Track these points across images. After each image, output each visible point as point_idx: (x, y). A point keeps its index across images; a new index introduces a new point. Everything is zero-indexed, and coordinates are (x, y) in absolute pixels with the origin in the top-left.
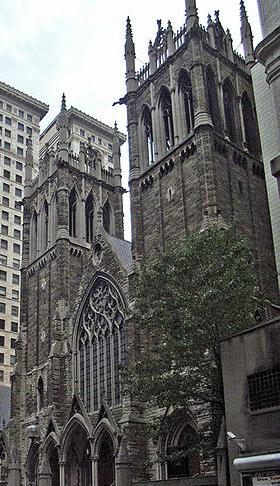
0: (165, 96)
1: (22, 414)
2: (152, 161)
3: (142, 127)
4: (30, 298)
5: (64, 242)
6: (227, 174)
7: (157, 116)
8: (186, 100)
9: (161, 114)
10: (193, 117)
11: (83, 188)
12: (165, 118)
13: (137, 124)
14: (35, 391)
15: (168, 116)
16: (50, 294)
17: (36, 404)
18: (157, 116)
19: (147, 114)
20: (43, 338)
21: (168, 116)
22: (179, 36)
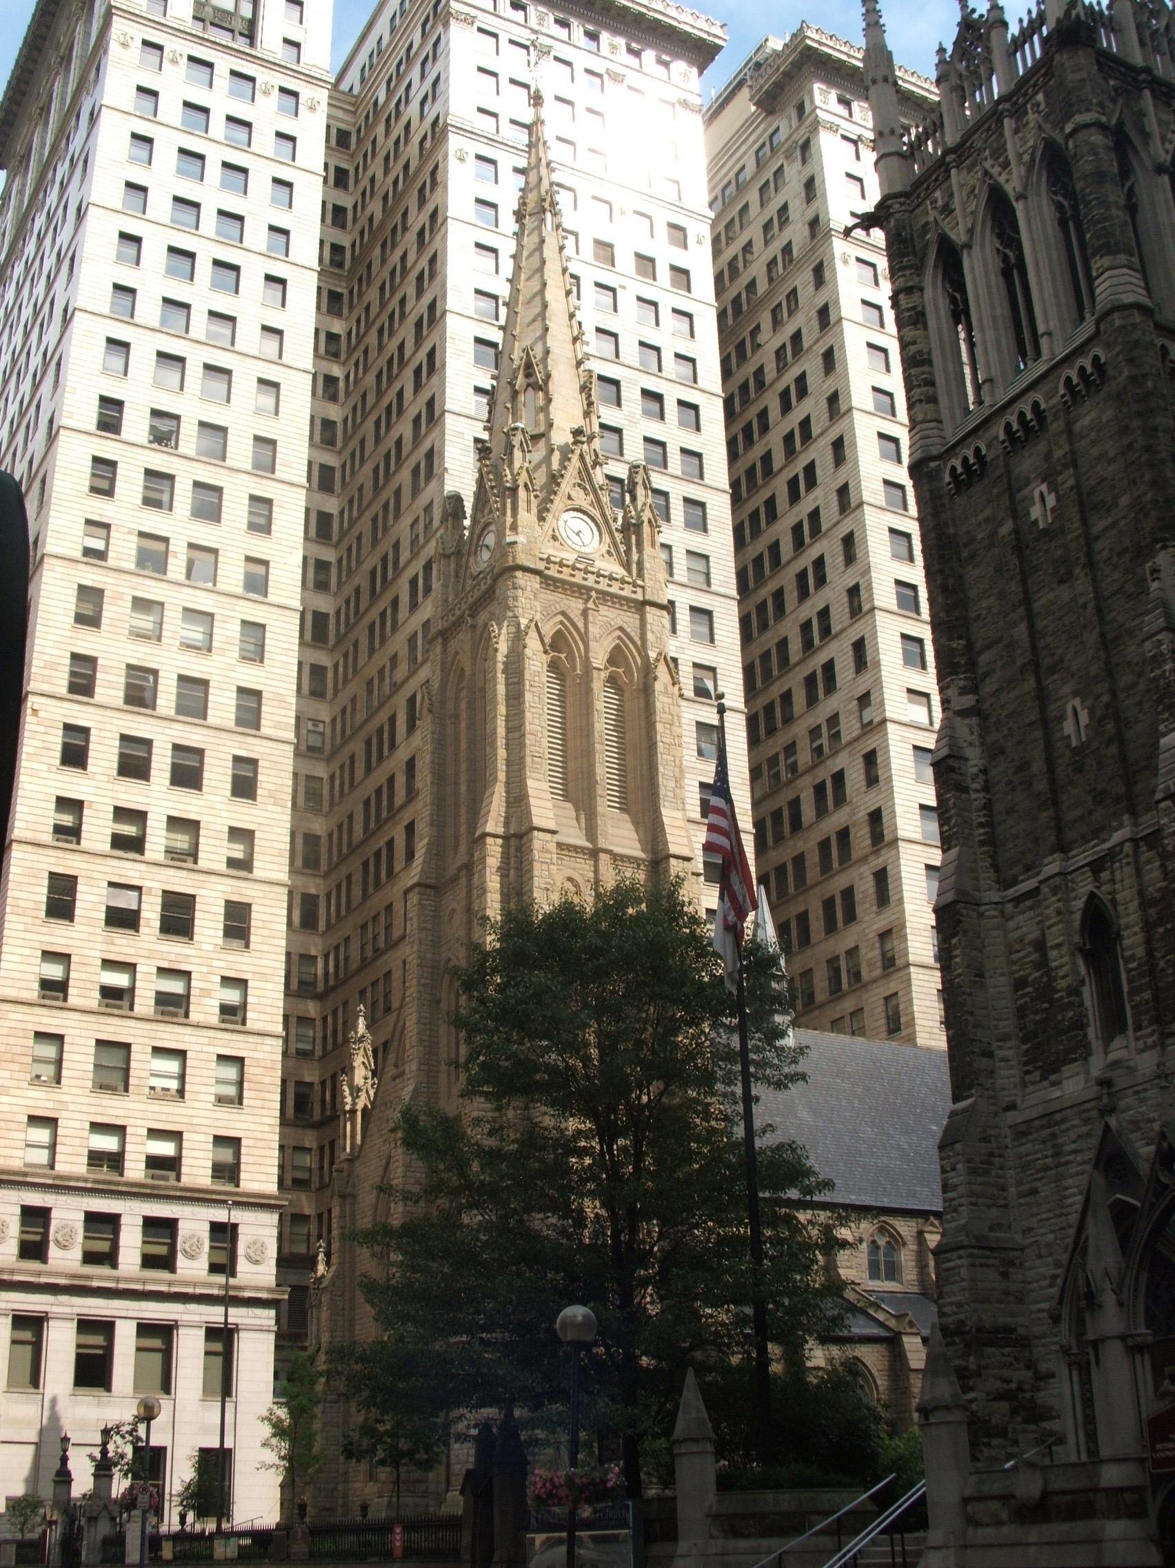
0: (1000, 209)
1: (1008, 1076)
2: (979, 402)
3: (934, 297)
4: (972, 573)
5: (1137, 318)
6: (591, 875)
7: (979, 268)
8: (1063, 223)
9: (995, 263)
10: (1090, 280)
11: (1152, 124)
12: (1006, 274)
13: (921, 290)
14: (1066, 964)
15: (1013, 269)
16: (1089, 540)
17: (1080, 1024)
18: (979, 268)
19: (950, 259)
20: (1076, 721)
21: (1013, 269)
22: (1026, 35)
